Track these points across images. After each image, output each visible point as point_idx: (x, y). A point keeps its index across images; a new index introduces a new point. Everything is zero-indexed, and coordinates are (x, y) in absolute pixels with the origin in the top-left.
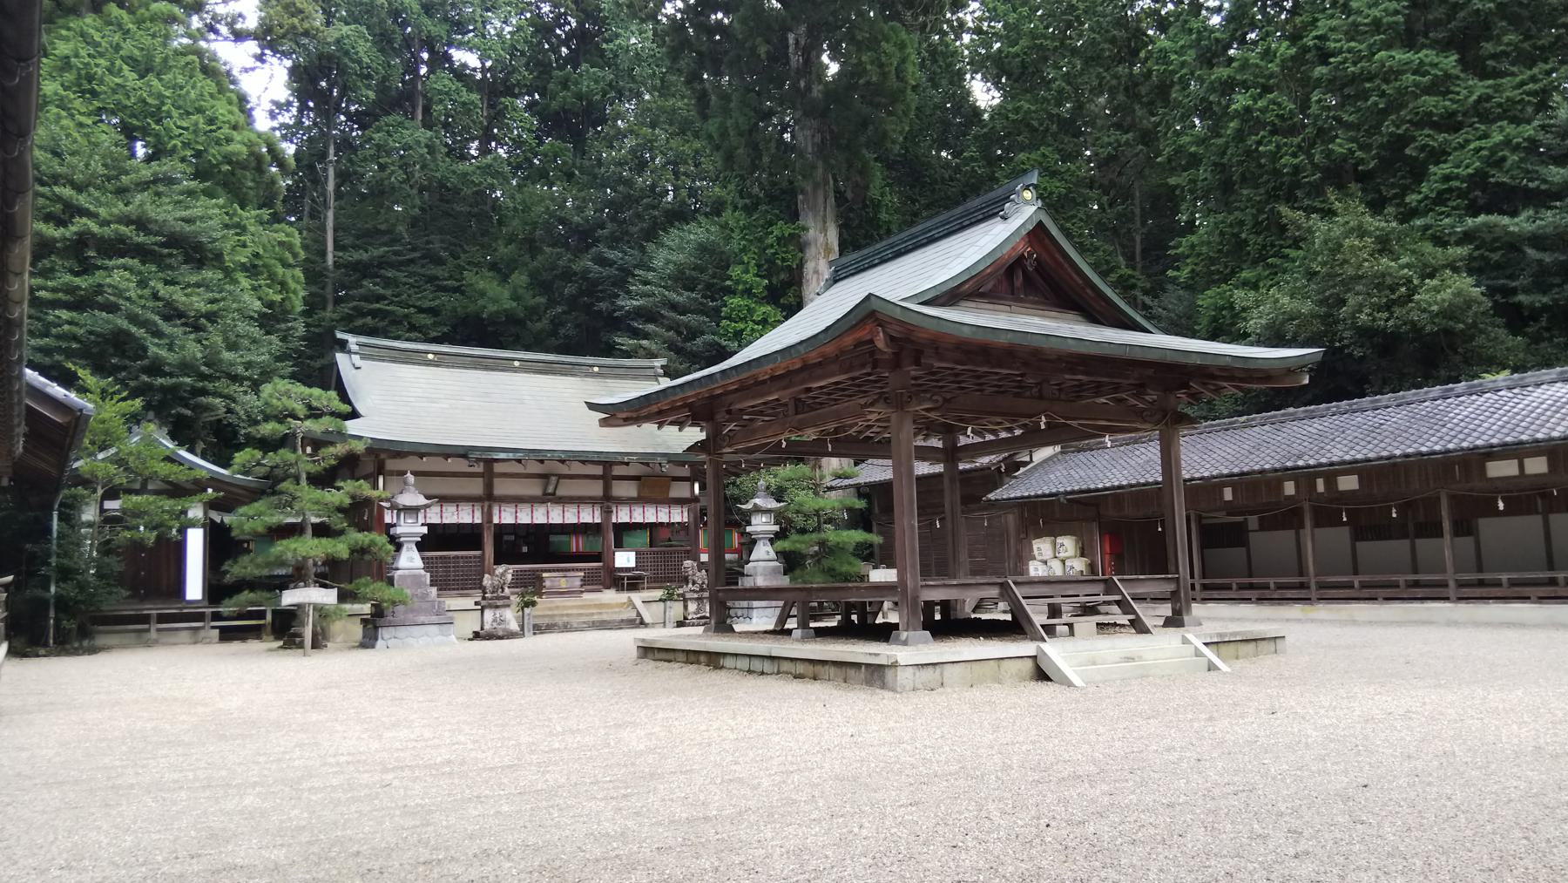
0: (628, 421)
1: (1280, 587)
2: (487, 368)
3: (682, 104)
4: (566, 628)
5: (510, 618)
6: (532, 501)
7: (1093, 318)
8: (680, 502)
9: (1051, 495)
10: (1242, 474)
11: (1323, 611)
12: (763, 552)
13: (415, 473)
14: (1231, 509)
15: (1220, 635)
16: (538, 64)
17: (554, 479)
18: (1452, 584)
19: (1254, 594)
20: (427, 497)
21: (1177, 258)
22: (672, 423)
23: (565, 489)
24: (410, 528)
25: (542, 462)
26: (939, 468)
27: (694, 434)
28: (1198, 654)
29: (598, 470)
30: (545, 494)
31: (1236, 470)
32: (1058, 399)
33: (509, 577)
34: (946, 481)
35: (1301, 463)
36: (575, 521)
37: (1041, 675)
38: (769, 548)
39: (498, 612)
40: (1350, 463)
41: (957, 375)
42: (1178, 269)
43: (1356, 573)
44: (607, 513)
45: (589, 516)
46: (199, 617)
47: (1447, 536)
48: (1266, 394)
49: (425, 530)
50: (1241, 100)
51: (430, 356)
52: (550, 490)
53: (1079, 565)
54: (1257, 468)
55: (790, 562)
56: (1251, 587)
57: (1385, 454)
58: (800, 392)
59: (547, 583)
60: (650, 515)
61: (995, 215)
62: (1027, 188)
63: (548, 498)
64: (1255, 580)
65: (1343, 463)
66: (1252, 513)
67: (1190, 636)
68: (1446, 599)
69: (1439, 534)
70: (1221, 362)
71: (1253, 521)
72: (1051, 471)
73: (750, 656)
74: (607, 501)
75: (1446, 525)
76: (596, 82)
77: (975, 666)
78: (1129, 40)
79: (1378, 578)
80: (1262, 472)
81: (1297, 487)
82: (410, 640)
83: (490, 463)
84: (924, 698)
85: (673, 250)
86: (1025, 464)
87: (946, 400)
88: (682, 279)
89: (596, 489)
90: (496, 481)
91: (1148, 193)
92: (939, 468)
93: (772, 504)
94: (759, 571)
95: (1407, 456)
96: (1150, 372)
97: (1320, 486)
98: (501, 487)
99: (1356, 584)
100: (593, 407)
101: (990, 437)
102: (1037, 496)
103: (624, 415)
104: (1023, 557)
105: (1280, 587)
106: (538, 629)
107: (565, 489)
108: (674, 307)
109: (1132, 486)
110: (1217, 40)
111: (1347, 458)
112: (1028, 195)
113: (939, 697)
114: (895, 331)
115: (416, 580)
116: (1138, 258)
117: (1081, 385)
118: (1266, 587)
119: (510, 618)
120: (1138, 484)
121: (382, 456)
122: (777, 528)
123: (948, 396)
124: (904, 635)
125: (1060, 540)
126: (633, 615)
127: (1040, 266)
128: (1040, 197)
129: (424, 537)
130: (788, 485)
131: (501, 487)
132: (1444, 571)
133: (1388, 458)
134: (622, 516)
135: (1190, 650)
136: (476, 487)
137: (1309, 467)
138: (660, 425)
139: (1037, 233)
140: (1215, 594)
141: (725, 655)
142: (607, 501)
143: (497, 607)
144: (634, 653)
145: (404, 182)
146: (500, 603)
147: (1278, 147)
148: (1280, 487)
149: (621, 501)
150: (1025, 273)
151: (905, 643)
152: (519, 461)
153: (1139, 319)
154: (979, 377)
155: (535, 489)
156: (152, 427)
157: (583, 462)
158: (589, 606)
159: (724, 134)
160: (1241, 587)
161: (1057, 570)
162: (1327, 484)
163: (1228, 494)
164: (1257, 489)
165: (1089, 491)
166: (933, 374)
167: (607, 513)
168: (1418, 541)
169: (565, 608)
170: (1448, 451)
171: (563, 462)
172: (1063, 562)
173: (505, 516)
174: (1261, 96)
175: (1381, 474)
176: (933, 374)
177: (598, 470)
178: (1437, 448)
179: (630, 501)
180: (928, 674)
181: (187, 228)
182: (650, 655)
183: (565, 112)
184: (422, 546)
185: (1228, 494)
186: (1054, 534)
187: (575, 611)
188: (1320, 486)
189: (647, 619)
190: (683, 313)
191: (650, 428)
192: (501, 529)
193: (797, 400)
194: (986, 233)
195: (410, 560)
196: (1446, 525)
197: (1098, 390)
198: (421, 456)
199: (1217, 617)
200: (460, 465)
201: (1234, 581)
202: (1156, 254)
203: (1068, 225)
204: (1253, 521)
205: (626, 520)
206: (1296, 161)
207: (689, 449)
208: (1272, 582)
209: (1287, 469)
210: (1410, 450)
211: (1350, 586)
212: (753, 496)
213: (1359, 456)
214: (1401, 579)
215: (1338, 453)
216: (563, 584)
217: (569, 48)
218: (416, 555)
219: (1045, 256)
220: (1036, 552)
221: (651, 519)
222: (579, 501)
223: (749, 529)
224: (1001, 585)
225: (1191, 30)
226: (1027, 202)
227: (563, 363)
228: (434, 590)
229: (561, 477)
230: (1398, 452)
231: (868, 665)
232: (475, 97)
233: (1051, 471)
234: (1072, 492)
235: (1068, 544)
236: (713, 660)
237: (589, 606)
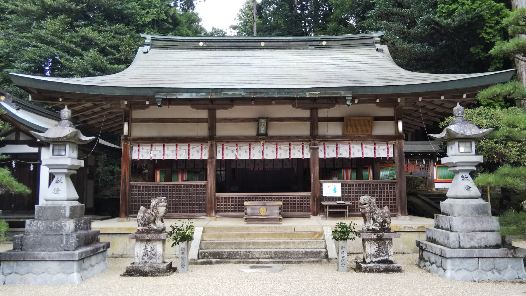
8: (385, 139)
23: (275, 130)
30: (258, 134)
38: (470, 182)
39: (149, 246)
44: (314, 150)
45: (299, 152)
51: (201, 44)
59: (249, 211)
60: (356, 151)
90: (218, 125)
94: (457, 210)
98: (222, 130)
107: (275, 130)
122: (479, 159)
131: (222, 130)
134: (329, 152)
136: (202, 130)
143: (148, 241)
146: (149, 237)
149: (326, 139)
155: (250, 131)
158: (280, 235)
167: (314, 150)
173: (229, 153)
179: (335, 139)
189: (332, 254)
192: (324, 162)
205: (333, 155)
216: (263, 211)
222: (289, 140)
229: (270, 120)
237: (280, 235)
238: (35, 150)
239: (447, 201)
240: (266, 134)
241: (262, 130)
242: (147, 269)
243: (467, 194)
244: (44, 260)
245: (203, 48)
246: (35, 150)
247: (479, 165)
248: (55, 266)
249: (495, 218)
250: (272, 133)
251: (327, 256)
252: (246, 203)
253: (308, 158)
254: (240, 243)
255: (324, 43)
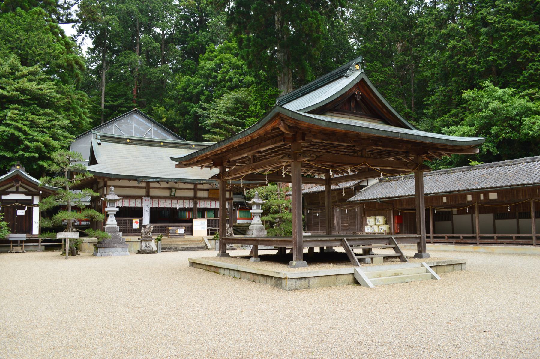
0: (186, 165)
1: (464, 238)
2: (150, 145)
3: (234, 44)
4: (176, 249)
5: (153, 245)
6: (165, 198)
7: (387, 123)
9: (374, 199)
10: (451, 192)
11: (482, 248)
12: (257, 222)
13: (114, 186)
14: (446, 206)
15: (438, 263)
16: (184, 32)
17: (174, 190)
18: (534, 238)
19: (454, 240)
20: (119, 196)
21: (427, 105)
22: (206, 166)
23: (179, 194)
24: (112, 209)
25: (167, 183)
26: (323, 188)
27: (216, 171)
28: (427, 271)
29: (192, 186)
30: (171, 196)
31: (448, 190)
32: (370, 157)
33: (152, 229)
34: (326, 193)
35: (474, 188)
36: (157, 206)
37: (356, 282)
40: (495, 188)
41: (325, 146)
42: (427, 109)
43: (495, 233)
44: (195, 204)
45: (188, 205)
46: (37, 241)
47: (533, 219)
48: (462, 157)
49: (118, 209)
50: (452, 43)
51: (128, 141)
52: (173, 194)
53: (385, 228)
54: (457, 189)
55: (269, 225)
56: (453, 238)
57: (509, 184)
58: (255, 153)
59: (171, 231)
61: (343, 76)
62: (357, 64)
63: (172, 197)
64: (455, 235)
65: (492, 188)
66: (454, 208)
67: (424, 264)
68: (532, 244)
69: (530, 217)
70: (440, 142)
71: (455, 211)
72: (376, 189)
73: (230, 269)
74: (195, 199)
75: (533, 214)
76: (205, 38)
77: (325, 278)
78: (410, 21)
79: (504, 235)
80: (459, 191)
81: (473, 197)
82: (111, 253)
83: (148, 183)
84: (299, 294)
85: (226, 100)
86: (365, 186)
87: (317, 157)
88: (229, 111)
89: (191, 194)
90: (151, 190)
91: (415, 79)
92: (323, 188)
93: (261, 201)
94: (254, 228)
95: (518, 185)
96: (410, 146)
97: (482, 197)
98: (153, 192)
99: (495, 238)
100: (173, 159)
101: (345, 174)
102: (369, 200)
103: (185, 163)
104: (363, 224)
105: (464, 238)
106: (164, 250)
108: (226, 122)
109: (406, 196)
110: (443, 19)
111: (494, 186)
112: (357, 67)
113: (305, 294)
114: (289, 123)
115: (112, 230)
116: (413, 106)
117: (381, 151)
118: (459, 238)
119: (153, 245)
120: (409, 195)
121: (106, 180)
122: (262, 211)
123: (319, 155)
124: (294, 263)
125: (378, 217)
126: (204, 245)
127: (363, 98)
128: (363, 68)
129: (117, 212)
130: (269, 193)
131: (153, 192)
132: (531, 233)
133: (510, 186)
134: (202, 205)
135: (423, 269)
137: (477, 189)
138: (202, 167)
139: (361, 84)
140: (439, 240)
141: (220, 268)
142: (195, 199)
143: (147, 241)
144: (188, 264)
145: (130, 76)
146: (147, 239)
147: (467, 62)
148: (466, 197)
150: (356, 101)
151: (295, 267)
152: (158, 182)
153: (406, 123)
154: (335, 147)
156: (18, 167)
157: (184, 183)
158: (186, 241)
159: (248, 55)
160: (449, 238)
161: (376, 230)
162: (484, 196)
163: (445, 200)
164: (456, 198)
165: (389, 198)
166: (314, 145)
167: (195, 204)
168: (520, 220)
169: (176, 241)
170: (535, 183)
171: (176, 183)
172: (379, 226)
174: (460, 41)
175: (505, 192)
176: (314, 145)
177: (192, 186)
178: (530, 182)
179: (204, 199)
180: (302, 282)
181: (40, 92)
182: (194, 265)
183: (193, 49)
184: (117, 215)
185: (445, 200)
186: (375, 215)
187: (180, 243)
188: (482, 197)
189: (209, 247)
190: (231, 125)
191: (197, 168)
192: (435, 198)
193: (254, 157)
194: (339, 83)
195: (112, 221)
196: (533, 214)
197: (389, 154)
198: (120, 180)
199: (438, 252)
200: (134, 183)
201: (446, 235)
202: (419, 106)
203: (385, 92)
204: (455, 211)
205: (169, 206)
206: (473, 67)
207: (211, 178)
208: (461, 236)
209: (469, 190)
210: (519, 183)
211: (493, 238)
212: (253, 197)
213: (498, 185)
214: (514, 236)
215: (488, 184)
217: (264, 70)
218: (114, 219)
219: (365, 94)
220: (368, 222)
221: (214, 206)
222: (184, 198)
223: (251, 211)
224: (341, 240)
225: (433, 14)
226: (357, 70)
227: (181, 144)
228: (121, 234)
229: (176, 189)
230: (514, 184)
231: (275, 277)
232: (158, 45)
233: (376, 189)
234: (383, 198)
235: (381, 219)
236: (216, 269)
237: (186, 241)
238: (30, 198)
239: (252, 225)
240: (174, 196)
241: (173, 194)
242: (148, 251)
243: (258, 223)
244: (116, 247)
245: (128, 143)
246: (30, 198)
247: (262, 213)
248: (120, 249)
249: (266, 231)
250: (177, 195)
251: (207, 248)
252: (170, 228)
253: (498, 219)
254: (171, 245)
255: (194, 146)
